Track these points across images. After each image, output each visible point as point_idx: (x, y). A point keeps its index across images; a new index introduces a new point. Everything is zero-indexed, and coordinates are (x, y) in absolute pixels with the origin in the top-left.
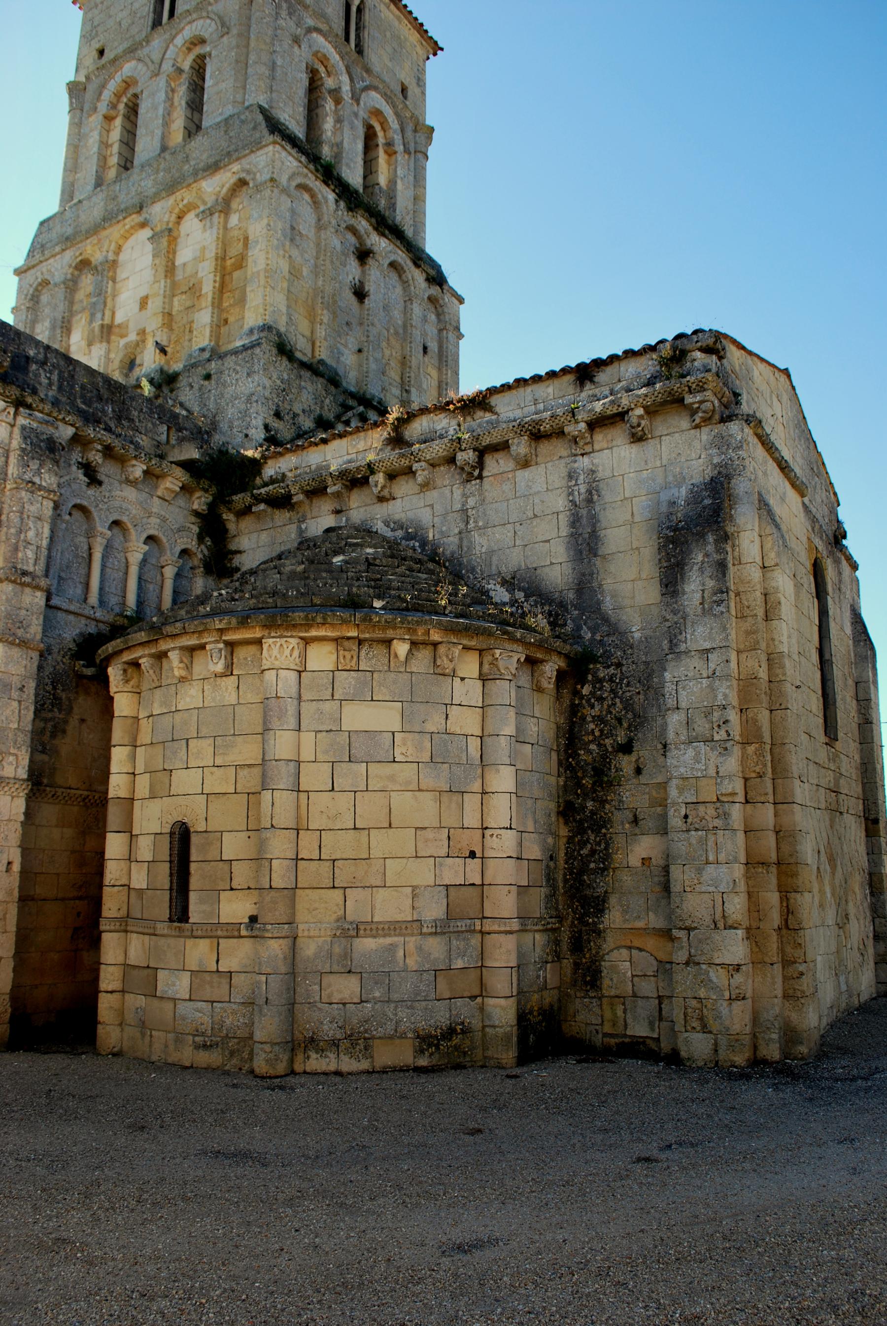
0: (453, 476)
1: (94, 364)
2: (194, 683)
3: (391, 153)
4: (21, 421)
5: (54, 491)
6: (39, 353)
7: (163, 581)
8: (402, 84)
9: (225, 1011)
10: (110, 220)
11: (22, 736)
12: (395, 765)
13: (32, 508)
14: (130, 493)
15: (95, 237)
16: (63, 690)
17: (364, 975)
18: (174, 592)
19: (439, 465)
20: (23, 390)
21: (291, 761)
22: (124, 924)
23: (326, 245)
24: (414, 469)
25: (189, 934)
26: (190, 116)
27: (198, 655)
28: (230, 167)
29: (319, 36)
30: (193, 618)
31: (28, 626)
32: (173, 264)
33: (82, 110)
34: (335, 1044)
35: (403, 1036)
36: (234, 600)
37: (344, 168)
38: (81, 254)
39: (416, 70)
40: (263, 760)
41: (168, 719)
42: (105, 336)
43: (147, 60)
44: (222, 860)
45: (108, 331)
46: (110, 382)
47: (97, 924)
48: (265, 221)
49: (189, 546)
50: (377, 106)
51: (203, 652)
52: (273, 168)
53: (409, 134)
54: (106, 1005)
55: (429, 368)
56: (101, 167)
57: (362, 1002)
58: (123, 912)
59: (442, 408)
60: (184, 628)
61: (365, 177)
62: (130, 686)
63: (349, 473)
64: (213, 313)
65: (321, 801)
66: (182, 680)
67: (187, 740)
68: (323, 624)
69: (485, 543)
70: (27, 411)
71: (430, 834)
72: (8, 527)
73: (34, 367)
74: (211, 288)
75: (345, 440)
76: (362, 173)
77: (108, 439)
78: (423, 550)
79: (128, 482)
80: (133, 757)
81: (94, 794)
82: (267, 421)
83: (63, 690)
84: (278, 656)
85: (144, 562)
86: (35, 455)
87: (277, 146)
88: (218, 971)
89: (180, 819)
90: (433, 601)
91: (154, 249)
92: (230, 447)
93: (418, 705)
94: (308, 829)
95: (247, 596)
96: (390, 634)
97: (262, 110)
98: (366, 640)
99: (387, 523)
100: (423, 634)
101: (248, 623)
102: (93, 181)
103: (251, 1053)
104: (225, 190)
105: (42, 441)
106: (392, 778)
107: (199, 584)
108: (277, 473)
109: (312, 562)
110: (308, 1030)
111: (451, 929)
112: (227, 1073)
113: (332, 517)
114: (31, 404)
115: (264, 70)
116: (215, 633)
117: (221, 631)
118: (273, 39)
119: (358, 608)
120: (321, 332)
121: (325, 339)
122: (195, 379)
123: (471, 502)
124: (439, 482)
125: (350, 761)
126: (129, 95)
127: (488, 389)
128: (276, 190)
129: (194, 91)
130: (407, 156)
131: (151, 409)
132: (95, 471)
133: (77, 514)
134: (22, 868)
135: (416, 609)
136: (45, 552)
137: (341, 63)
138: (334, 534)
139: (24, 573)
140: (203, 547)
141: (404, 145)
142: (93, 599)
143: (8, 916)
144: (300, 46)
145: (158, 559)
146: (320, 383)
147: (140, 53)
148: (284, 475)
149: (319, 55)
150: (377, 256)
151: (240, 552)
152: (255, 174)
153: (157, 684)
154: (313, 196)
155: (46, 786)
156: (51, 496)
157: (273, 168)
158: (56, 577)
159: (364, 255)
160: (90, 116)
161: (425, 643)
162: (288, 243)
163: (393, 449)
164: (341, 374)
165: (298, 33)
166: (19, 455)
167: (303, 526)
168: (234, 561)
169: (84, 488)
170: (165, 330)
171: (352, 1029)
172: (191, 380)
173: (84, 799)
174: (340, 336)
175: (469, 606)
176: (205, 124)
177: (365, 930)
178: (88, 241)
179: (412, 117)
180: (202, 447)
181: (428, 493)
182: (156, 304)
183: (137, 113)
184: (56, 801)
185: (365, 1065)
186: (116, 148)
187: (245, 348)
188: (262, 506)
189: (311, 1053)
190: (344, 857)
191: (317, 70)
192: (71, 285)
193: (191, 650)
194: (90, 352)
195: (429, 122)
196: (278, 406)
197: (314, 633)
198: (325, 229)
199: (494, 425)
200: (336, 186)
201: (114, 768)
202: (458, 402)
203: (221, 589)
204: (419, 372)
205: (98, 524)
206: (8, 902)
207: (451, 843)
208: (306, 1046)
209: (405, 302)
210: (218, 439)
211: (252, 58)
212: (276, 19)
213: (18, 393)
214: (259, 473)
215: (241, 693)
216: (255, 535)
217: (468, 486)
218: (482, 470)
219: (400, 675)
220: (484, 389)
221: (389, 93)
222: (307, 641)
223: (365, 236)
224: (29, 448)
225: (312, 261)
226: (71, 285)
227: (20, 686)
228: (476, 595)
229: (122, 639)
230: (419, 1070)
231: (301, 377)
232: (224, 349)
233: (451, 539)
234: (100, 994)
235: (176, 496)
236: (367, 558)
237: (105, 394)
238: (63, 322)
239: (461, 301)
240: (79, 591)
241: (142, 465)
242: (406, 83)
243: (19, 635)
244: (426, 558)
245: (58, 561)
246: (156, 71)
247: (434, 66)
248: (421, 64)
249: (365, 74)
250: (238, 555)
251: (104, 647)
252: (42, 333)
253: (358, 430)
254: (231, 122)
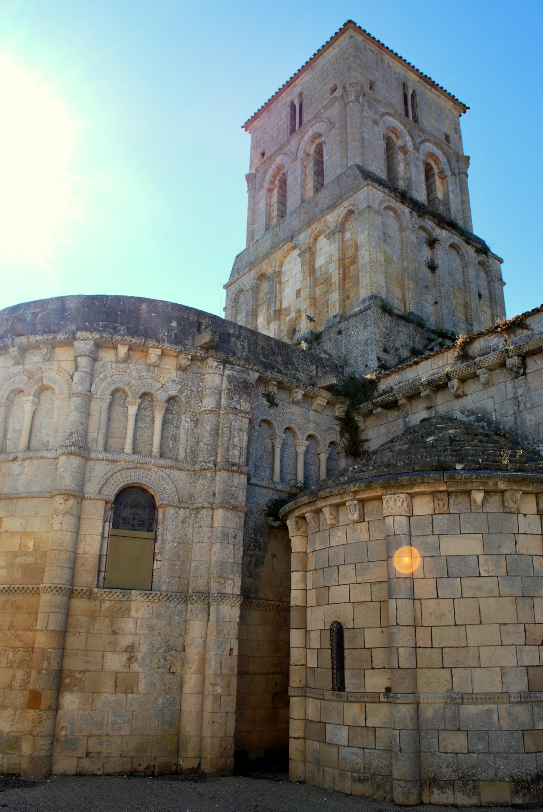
0: (505, 376)
1: (271, 334)
2: (340, 528)
3: (443, 177)
4: (227, 372)
5: (248, 413)
6: (236, 331)
7: (320, 463)
8: (446, 134)
9: (372, 755)
10: (275, 248)
11: (236, 567)
12: (481, 579)
13: (237, 424)
14: (296, 409)
15: (267, 259)
16: (261, 537)
17: (469, 732)
18: (327, 469)
19: (495, 369)
20: (228, 353)
21: (407, 578)
22: (303, 691)
23: (407, 240)
24: (477, 374)
25: (345, 699)
26: (316, 179)
27: (341, 508)
28: (343, 204)
29: (389, 117)
30: (337, 485)
31: (237, 497)
32: (314, 267)
33: (255, 189)
34: (451, 783)
35: (501, 780)
36: (362, 471)
37: (414, 192)
38: (260, 271)
39: (453, 124)
40: (389, 578)
41: (325, 552)
42: (277, 316)
43: (289, 153)
44: (365, 648)
45: (278, 314)
46: (279, 343)
47: (287, 691)
48: (367, 232)
49: (335, 440)
50: (431, 151)
51: (345, 507)
52: (369, 200)
53: (454, 163)
54: (294, 746)
55: (484, 308)
56: (268, 219)
57: (469, 752)
58: (303, 683)
59: (493, 331)
60: (331, 492)
61: (428, 195)
62: (300, 532)
63: (434, 382)
64: (340, 293)
65: (430, 606)
66: (332, 526)
67: (338, 566)
68: (422, 483)
69: (533, 418)
70: (230, 366)
71: (510, 628)
72: (223, 437)
73: (233, 339)
74: (338, 278)
75: (429, 361)
76: (425, 192)
77: (280, 377)
78: (489, 427)
79: (294, 402)
80: (305, 578)
81: (283, 603)
82: (379, 355)
83: (261, 537)
84: (394, 507)
85: (307, 452)
86: (236, 392)
87: (370, 186)
88: (366, 726)
89: (336, 620)
90: (498, 462)
91: (302, 261)
92: (356, 374)
93: (494, 535)
94: (422, 626)
95: (371, 468)
96: (469, 486)
97: (358, 167)
98: (453, 492)
99: (463, 412)
100: (493, 485)
101: (372, 486)
102: (264, 228)
103: (392, 787)
104: (340, 218)
105: (240, 383)
106: (479, 588)
107: (343, 463)
108: (387, 387)
109: (413, 442)
110: (431, 772)
111: (533, 699)
112: (375, 801)
113: (426, 411)
114: (232, 362)
115: (357, 144)
116: (351, 494)
117: (355, 493)
118: (361, 125)
119: (445, 470)
120: (409, 295)
121: (412, 299)
122: (332, 334)
123: (520, 392)
124: (496, 381)
125: (448, 577)
126: (280, 175)
127: (523, 314)
128: (371, 213)
129: (318, 165)
130: (454, 178)
131: (305, 356)
132: (273, 398)
133: (264, 425)
134: (239, 652)
135: (486, 468)
136: (245, 451)
137: (405, 130)
138: (427, 423)
139: (233, 464)
140: (344, 439)
141: (451, 171)
142: (277, 478)
143: (231, 684)
144: (378, 126)
145: (316, 449)
146: (411, 328)
147: (284, 150)
148: (392, 388)
149: (391, 128)
150: (441, 242)
151: (367, 440)
152: (358, 206)
153: (317, 530)
154: (395, 212)
155: (253, 599)
156: (247, 416)
157: (369, 200)
158: (254, 465)
159: (432, 243)
160: (260, 191)
161: (495, 492)
162: (382, 243)
163: (462, 363)
164: (424, 319)
165: (376, 118)
166: (227, 393)
167: (407, 420)
168: (364, 447)
169: (267, 409)
170: (312, 308)
171: (463, 773)
172: (330, 336)
173: (277, 607)
174: (421, 295)
175: (525, 463)
176: (326, 182)
177: (468, 699)
178: (264, 262)
179: (454, 153)
180: (338, 376)
181: (489, 389)
182: (305, 294)
183: (286, 184)
184: (260, 608)
185: (474, 800)
186: (275, 207)
187: (361, 311)
188: (379, 410)
189: (434, 789)
190: (449, 645)
191: (390, 138)
192: (256, 290)
193: (337, 507)
194: (269, 327)
195: (466, 153)
196: (386, 345)
197: (416, 490)
198: (405, 231)
199: (530, 337)
200: (409, 204)
201: (293, 587)
202: (503, 326)
203: (354, 465)
204: (477, 311)
205: (277, 431)
206: (231, 676)
207: (527, 635)
208: (430, 784)
209: (463, 267)
210: (348, 370)
211: (350, 138)
212: (362, 113)
213: (224, 356)
214: (376, 389)
215: (371, 533)
216: (376, 428)
217: (517, 381)
218: (525, 369)
219: (479, 515)
220: (520, 314)
221: (437, 142)
222: (412, 496)
223: (432, 231)
224: (232, 388)
225: (399, 252)
226: (256, 290)
227: (234, 535)
228: (529, 455)
229: (294, 502)
230: (514, 806)
231: (398, 325)
232: (348, 314)
233: (508, 418)
234: (290, 740)
235: (324, 409)
236: (450, 437)
237: (276, 350)
238: (252, 312)
239: (501, 261)
240: (268, 473)
241: (301, 391)
242: (448, 133)
243: (232, 503)
244: (492, 433)
245: (254, 455)
246: (295, 158)
247: (464, 120)
248: (456, 120)
249: (421, 134)
250: (367, 443)
251: (283, 508)
252: (241, 321)
253: (437, 353)
254: (341, 178)
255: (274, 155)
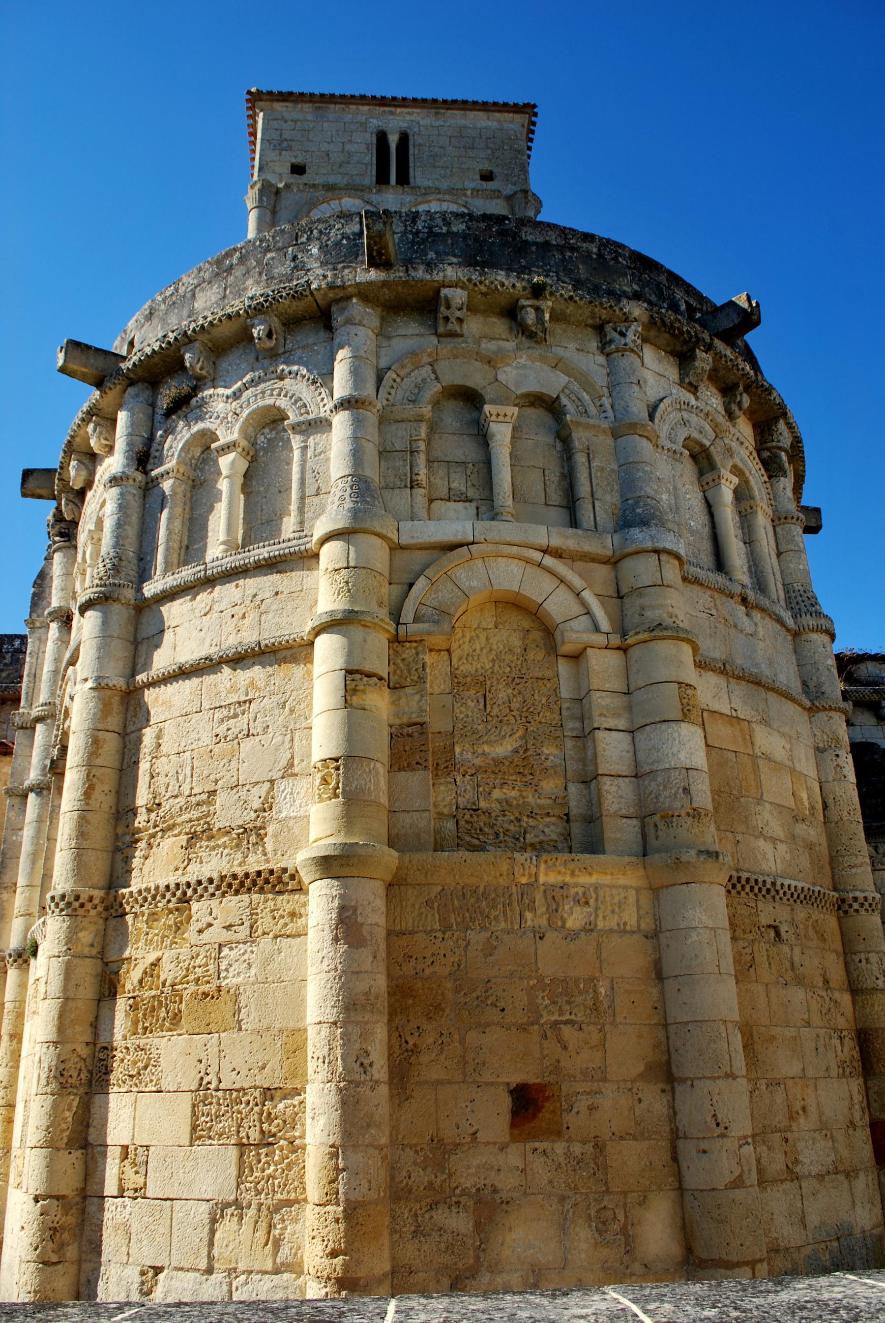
255: (340, 189)
